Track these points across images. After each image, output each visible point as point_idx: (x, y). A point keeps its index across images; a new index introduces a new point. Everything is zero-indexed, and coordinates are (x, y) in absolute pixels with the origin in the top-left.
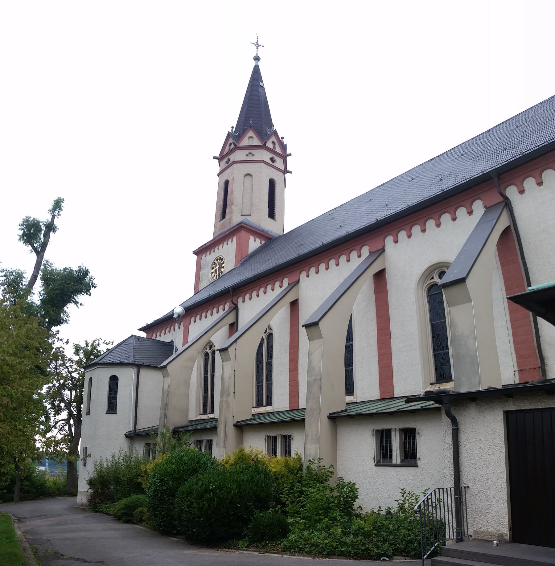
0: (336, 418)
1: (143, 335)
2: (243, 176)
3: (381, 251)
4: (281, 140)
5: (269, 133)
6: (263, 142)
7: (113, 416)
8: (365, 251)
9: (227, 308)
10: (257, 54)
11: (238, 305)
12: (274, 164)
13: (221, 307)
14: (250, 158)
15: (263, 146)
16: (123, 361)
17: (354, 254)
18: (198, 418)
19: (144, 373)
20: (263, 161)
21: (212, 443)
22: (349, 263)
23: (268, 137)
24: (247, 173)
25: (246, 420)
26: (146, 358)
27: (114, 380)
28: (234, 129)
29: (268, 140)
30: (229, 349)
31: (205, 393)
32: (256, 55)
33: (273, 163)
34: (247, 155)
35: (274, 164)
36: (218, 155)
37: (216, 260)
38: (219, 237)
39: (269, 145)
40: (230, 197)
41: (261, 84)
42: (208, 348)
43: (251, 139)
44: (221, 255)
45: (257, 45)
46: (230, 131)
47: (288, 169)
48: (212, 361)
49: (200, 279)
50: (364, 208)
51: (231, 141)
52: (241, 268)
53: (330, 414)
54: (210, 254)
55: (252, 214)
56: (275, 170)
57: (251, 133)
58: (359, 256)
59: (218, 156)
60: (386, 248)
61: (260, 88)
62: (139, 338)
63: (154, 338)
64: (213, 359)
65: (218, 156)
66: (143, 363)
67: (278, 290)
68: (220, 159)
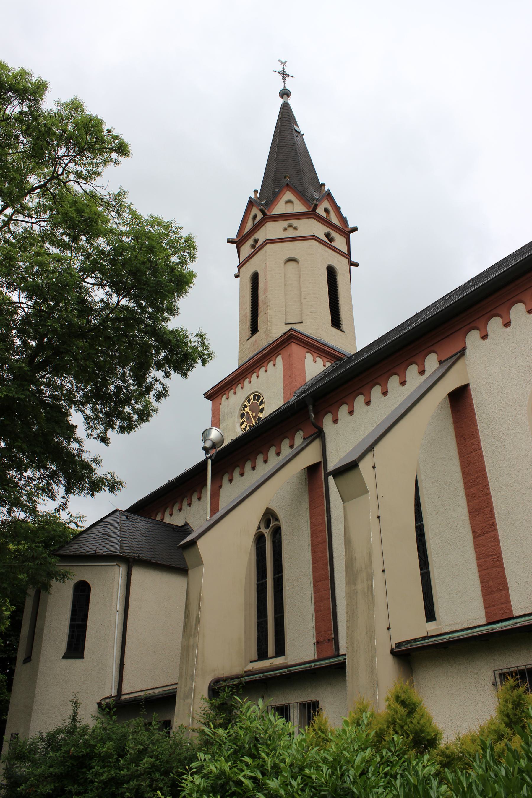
2: (282, 261)
10: (285, 87)
12: (333, 244)
14: (291, 233)
15: (312, 214)
18: (250, 667)
20: (314, 238)
28: (258, 194)
32: (283, 88)
33: (331, 242)
34: (285, 229)
36: (234, 236)
38: (251, 362)
40: (264, 297)
41: (296, 128)
44: (255, 390)
45: (284, 75)
55: (304, 321)
56: (335, 253)
59: (235, 237)
61: (295, 134)
65: (235, 237)
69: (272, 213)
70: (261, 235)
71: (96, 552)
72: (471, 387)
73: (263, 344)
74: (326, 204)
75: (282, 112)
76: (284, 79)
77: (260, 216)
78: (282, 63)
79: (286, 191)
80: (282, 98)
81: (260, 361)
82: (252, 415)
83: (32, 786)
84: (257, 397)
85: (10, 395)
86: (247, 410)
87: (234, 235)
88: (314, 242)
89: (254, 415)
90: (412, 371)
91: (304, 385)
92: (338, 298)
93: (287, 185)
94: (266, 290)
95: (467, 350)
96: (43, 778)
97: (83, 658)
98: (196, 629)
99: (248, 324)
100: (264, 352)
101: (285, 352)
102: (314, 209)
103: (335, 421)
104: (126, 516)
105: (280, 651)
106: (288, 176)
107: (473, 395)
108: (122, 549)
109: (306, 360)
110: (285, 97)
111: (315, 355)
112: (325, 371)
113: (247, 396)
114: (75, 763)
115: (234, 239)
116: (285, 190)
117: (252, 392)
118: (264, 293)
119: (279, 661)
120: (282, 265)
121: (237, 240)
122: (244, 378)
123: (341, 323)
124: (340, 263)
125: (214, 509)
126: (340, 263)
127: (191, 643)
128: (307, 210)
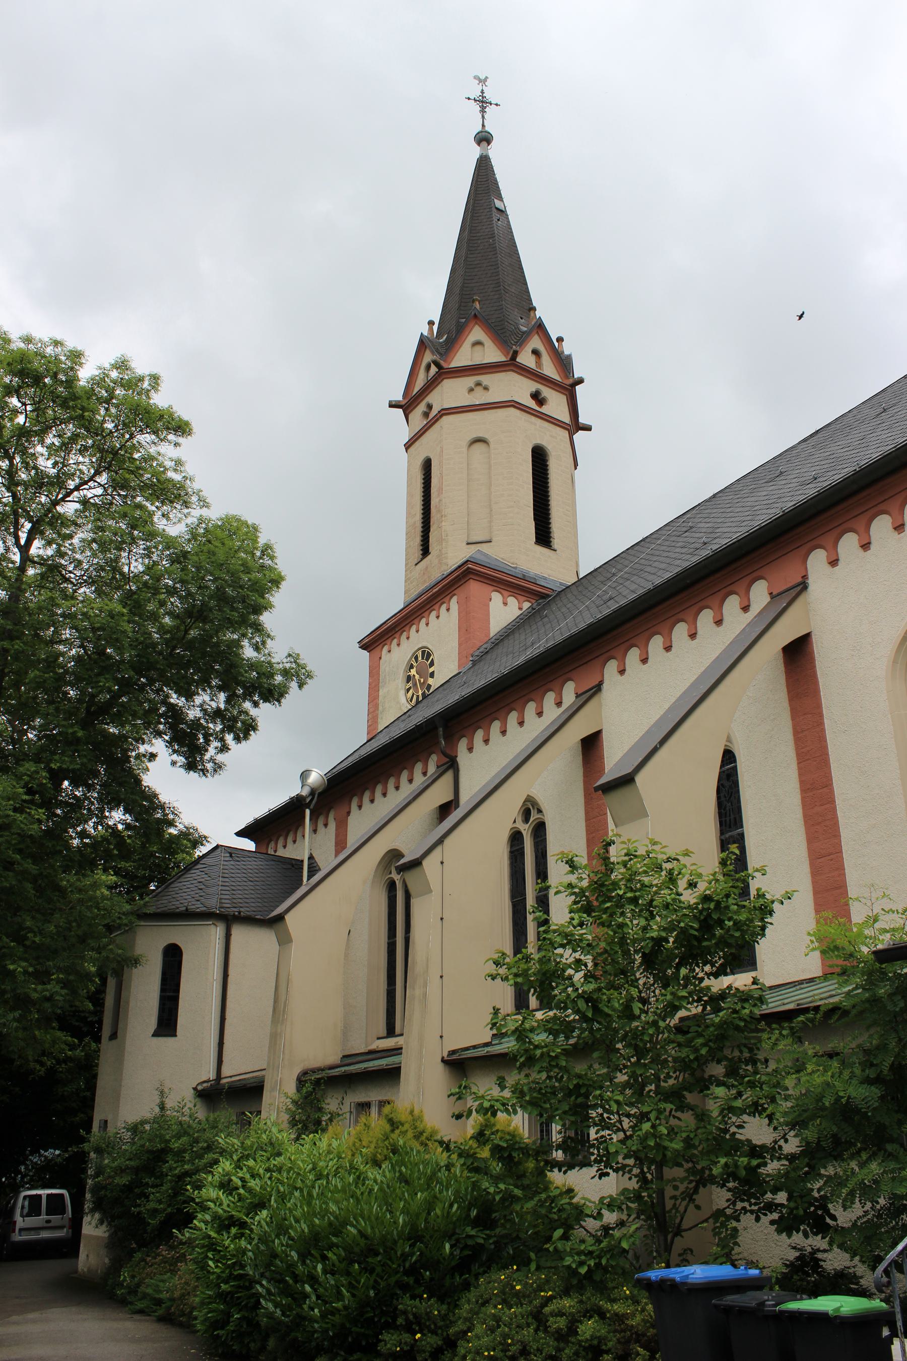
1: (248, 845)
2: (465, 444)
3: (799, 588)
4: (556, 344)
5: (525, 329)
6: (508, 353)
7: (169, 1041)
8: (760, 594)
9: (432, 769)
10: (483, 126)
11: (458, 759)
12: (544, 409)
13: (419, 767)
14: (479, 398)
15: (512, 364)
17: (732, 604)
19: (239, 933)
22: (721, 628)
23: (523, 339)
25: (474, 1047)
28: (435, 328)
29: (520, 345)
30: (425, 863)
32: (480, 128)
34: (471, 390)
35: (544, 409)
36: (398, 397)
38: (418, 602)
39: (526, 358)
40: (437, 500)
41: (498, 204)
43: (478, 348)
44: (424, 644)
45: (483, 103)
46: (426, 333)
47: (582, 420)
49: (380, 708)
50: (765, 493)
51: (428, 357)
52: (472, 670)
54: (398, 645)
55: (494, 539)
56: (546, 424)
57: (477, 333)
58: (746, 609)
59: (401, 398)
60: (810, 581)
62: (232, 852)
63: (271, 852)
65: (401, 398)
66: (240, 912)
67: (552, 713)
68: (407, 406)
69: (452, 365)
71: (187, 910)
73: (436, 575)
75: (478, 175)
76: (483, 111)
78: (480, 81)
79: (473, 327)
80: (479, 145)
81: (426, 605)
82: (420, 681)
83: (110, 1177)
84: (427, 654)
85: (64, 766)
86: (413, 672)
87: (398, 396)
89: (422, 680)
91: (486, 643)
92: (548, 496)
93: (475, 316)
94: (440, 490)
96: (121, 1171)
97: (176, 1036)
98: (283, 1015)
99: (418, 539)
101: (462, 592)
102: (515, 354)
106: (477, 300)
108: (221, 903)
109: (492, 604)
110: (484, 144)
111: (506, 593)
113: (413, 651)
114: (151, 1157)
115: (399, 401)
116: (471, 325)
118: (439, 495)
120: (465, 449)
122: (410, 624)
125: (340, 844)
127: (279, 1031)
128: (504, 359)
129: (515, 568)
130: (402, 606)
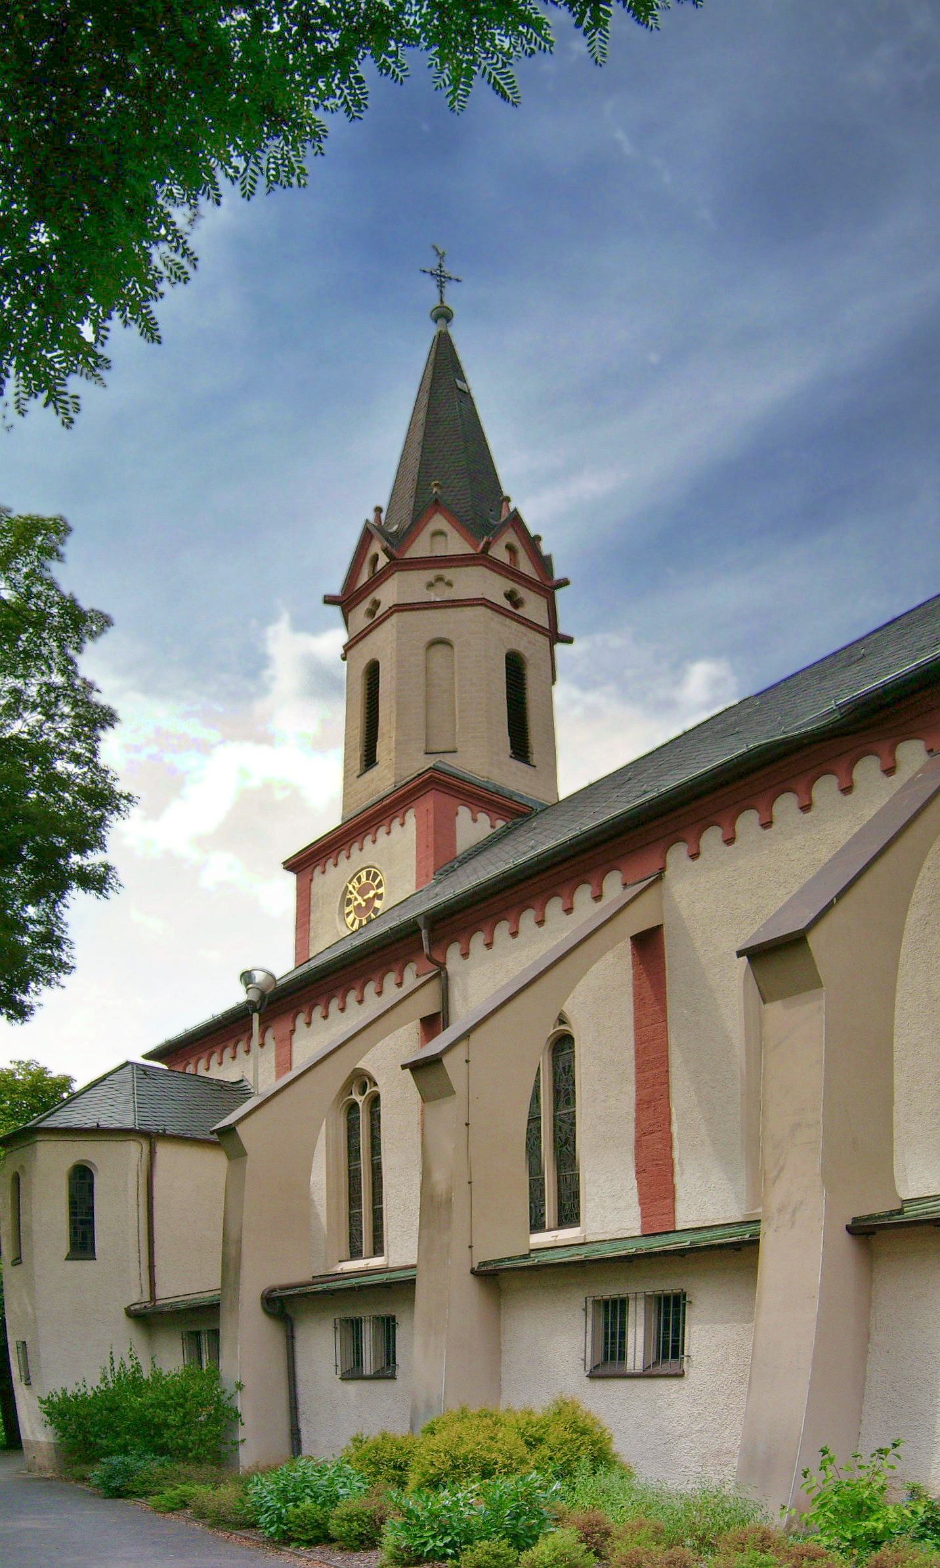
0: (874, 1233)
2: (422, 644)
10: (442, 301)
12: (519, 612)
15: (481, 559)
16: (104, 1124)
19: (164, 1151)
21: (394, 1326)
22: (850, 797)
24: (428, 639)
25: (509, 1259)
26: (171, 1119)
27: (82, 1178)
28: (383, 516)
31: (351, 1208)
32: (438, 304)
34: (430, 585)
37: (355, 880)
41: (460, 384)
42: (355, 1089)
43: (439, 538)
44: (370, 863)
48: (372, 1125)
49: (312, 934)
51: (376, 547)
53: (855, 1220)
56: (522, 628)
57: (439, 522)
64: (372, 1120)
68: (346, 601)
69: (407, 556)
70: (388, 594)
72: (666, 931)
74: (510, 537)
76: (441, 286)
77: (383, 560)
88: (482, 610)
90: (583, 894)
95: (666, 873)
99: (358, 754)
100: (384, 803)
102: (488, 546)
103: (465, 955)
104: (143, 1070)
105: (378, 1250)
107: (666, 941)
110: (441, 321)
112: (494, 835)
117: (365, 866)
119: (376, 1262)
120: (422, 651)
121: (341, 600)
123: (530, 750)
124: (530, 645)
125: (284, 1064)
126: (530, 645)
128: (472, 551)
129: (487, 782)
130: (340, 823)
